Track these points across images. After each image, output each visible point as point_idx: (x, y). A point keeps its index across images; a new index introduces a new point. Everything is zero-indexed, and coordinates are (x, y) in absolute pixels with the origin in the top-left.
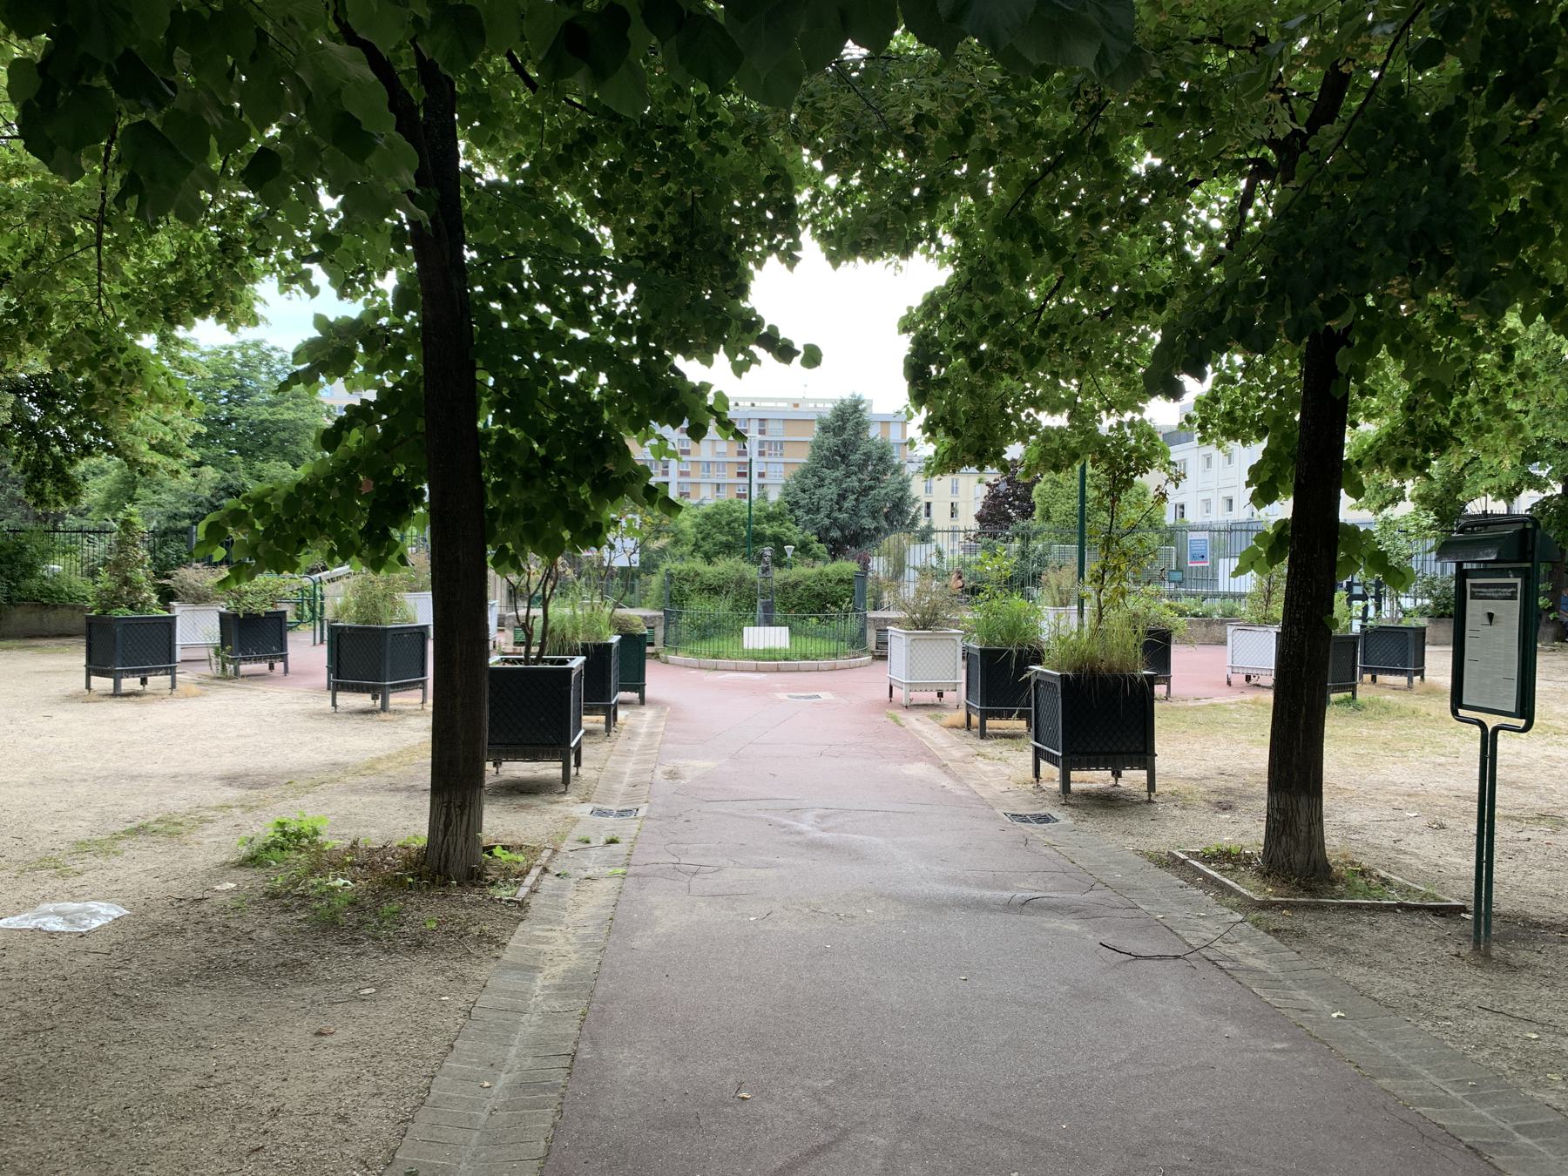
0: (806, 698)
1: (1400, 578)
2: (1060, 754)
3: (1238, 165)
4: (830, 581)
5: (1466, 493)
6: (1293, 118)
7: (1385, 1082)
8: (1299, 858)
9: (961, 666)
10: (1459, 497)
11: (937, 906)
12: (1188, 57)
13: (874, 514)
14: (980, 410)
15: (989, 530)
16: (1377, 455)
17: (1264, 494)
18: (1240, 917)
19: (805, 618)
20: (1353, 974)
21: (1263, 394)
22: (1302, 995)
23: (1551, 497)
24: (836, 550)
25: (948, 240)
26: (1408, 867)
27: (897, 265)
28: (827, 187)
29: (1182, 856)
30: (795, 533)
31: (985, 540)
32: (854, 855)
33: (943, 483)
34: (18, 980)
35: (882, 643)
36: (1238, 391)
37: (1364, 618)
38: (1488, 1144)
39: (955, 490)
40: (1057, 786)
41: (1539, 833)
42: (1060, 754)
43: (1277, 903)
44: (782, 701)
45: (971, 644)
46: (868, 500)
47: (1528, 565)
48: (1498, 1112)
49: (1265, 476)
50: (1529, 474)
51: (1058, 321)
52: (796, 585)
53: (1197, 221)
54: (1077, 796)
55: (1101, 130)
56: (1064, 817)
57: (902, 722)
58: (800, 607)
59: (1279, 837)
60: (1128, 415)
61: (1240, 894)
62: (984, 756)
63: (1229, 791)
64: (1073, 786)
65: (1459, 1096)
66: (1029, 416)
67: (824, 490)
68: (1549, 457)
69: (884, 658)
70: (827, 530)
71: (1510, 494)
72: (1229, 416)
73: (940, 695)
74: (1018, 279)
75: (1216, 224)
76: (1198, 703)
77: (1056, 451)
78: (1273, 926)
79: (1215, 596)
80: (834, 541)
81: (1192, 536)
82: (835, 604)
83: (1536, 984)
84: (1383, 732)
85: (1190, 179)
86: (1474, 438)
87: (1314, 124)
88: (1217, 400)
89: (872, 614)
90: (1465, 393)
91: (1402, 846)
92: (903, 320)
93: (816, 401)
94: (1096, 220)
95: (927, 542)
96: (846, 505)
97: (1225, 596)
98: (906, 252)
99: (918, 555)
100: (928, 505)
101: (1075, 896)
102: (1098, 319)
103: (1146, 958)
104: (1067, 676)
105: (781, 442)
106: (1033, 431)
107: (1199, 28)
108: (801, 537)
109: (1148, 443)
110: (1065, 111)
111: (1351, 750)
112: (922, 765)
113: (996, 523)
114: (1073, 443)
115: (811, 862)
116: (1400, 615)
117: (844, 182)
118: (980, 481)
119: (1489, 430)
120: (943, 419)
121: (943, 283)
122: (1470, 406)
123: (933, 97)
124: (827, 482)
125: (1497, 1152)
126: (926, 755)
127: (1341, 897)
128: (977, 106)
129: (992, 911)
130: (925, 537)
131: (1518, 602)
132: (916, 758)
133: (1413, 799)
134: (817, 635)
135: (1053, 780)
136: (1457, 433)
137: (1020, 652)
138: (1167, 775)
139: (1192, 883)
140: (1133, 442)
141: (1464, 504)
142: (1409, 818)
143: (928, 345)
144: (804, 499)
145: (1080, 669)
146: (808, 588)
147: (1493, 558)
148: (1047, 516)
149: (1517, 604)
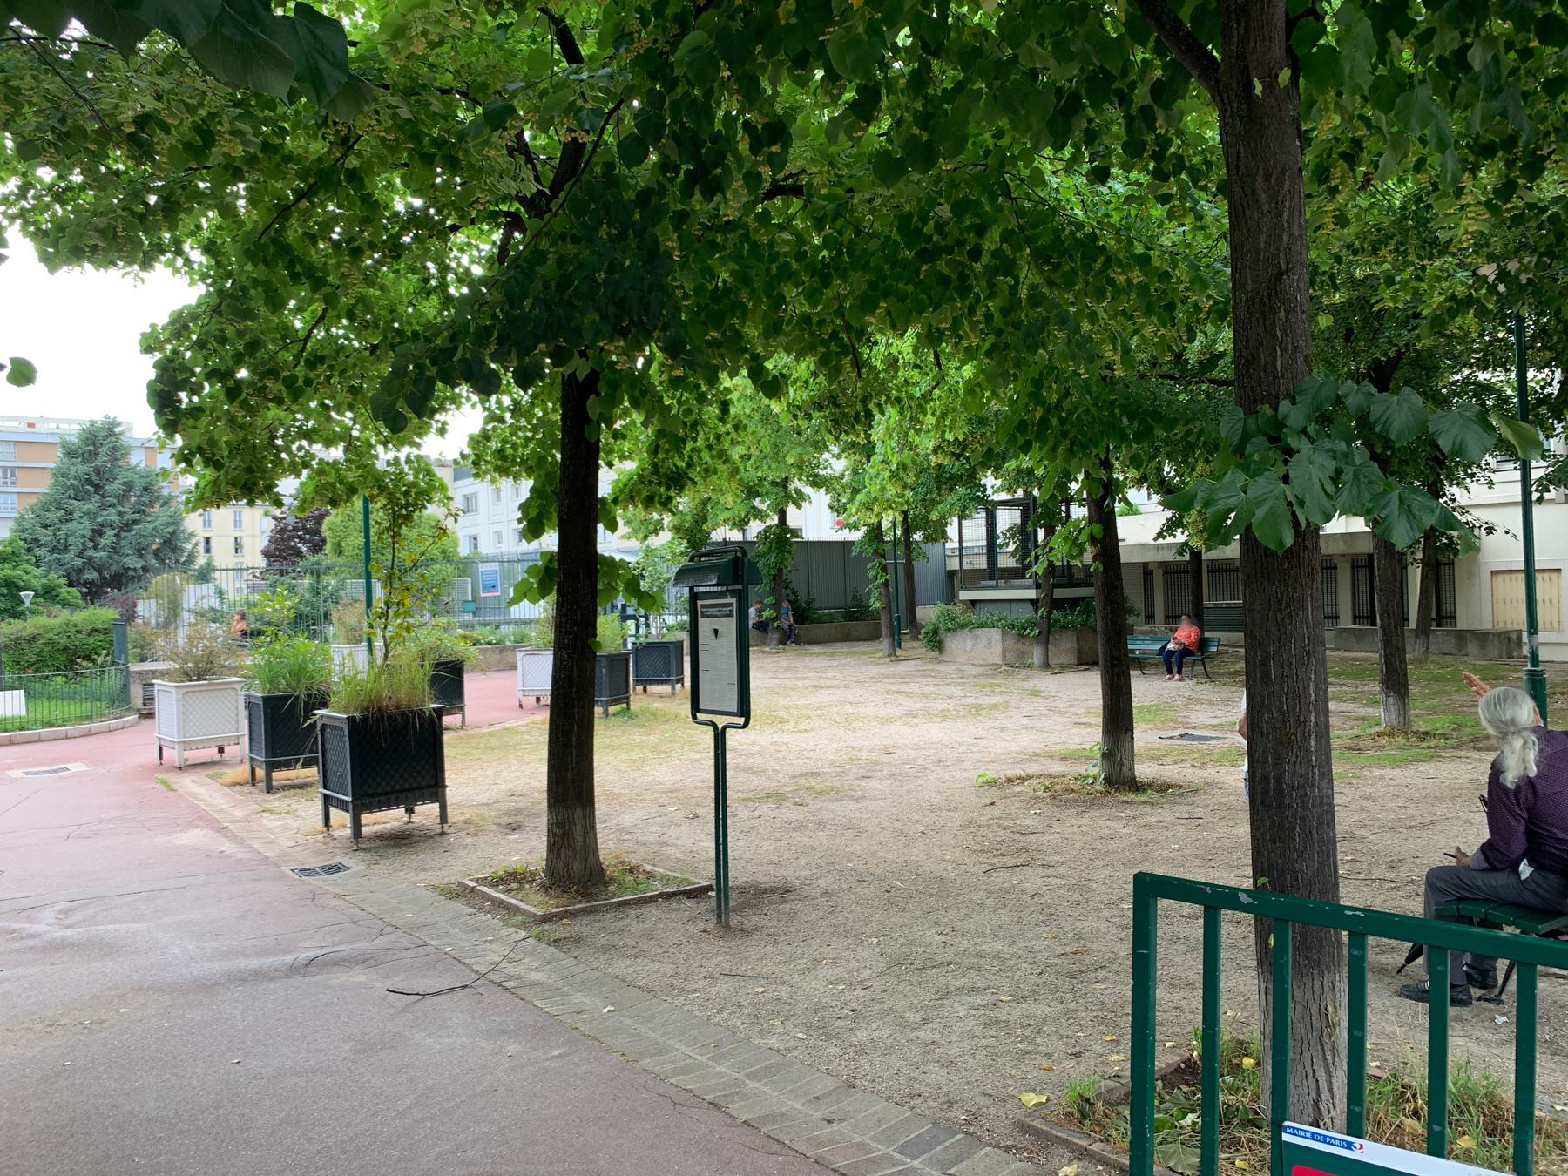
0: (37, 773)
1: (650, 601)
2: (349, 799)
3: (493, 217)
4: (79, 632)
5: (709, 524)
6: (537, 179)
7: (645, 1063)
8: (577, 867)
9: (243, 714)
10: (705, 527)
11: (208, 987)
12: (436, 106)
13: (140, 552)
14: (245, 440)
15: (277, 565)
16: (629, 493)
17: (533, 529)
18: (523, 934)
19: (47, 678)
20: (622, 967)
21: (530, 434)
22: (578, 998)
23: (770, 527)
24: (93, 593)
25: (197, 256)
26: (669, 857)
27: (136, 275)
28: (40, 180)
29: (472, 884)
30: (37, 577)
31: (271, 578)
32: (108, 949)
33: (223, 517)
34: (1060, 699)
35: (149, 699)
36: (508, 431)
37: (637, 635)
38: (725, 1096)
39: (238, 523)
40: (348, 832)
41: (767, 810)
42: (349, 799)
43: (557, 913)
44: (16, 779)
45: (252, 693)
46: (132, 535)
47: (740, 587)
48: (733, 1065)
49: (533, 513)
50: (754, 507)
51: (326, 352)
52: (32, 639)
53: (459, 264)
54: (369, 839)
55: (353, 162)
56: (355, 864)
57: (175, 786)
58: (40, 664)
59: (559, 850)
60: (406, 450)
61: (524, 912)
62: (271, 812)
63: (518, 811)
64: (365, 830)
65: (704, 1059)
66: (300, 448)
67: (73, 525)
68: (767, 493)
69: (151, 715)
70: (80, 571)
71: (741, 524)
72: (500, 453)
73: (221, 750)
74: (277, 304)
75: (477, 271)
76: (492, 729)
77: (333, 485)
78: (554, 937)
79: (508, 623)
80: (89, 584)
81: (482, 567)
82: (87, 658)
83: (763, 943)
84: (652, 737)
85: (449, 223)
86: (704, 479)
87: (556, 186)
88: (488, 439)
89: (135, 667)
90: (695, 440)
91: (665, 839)
92: (144, 336)
93: (58, 421)
94: (357, 253)
95: (207, 581)
96: (102, 542)
97: (517, 623)
98: (146, 264)
99: (195, 596)
100: (208, 540)
101: (365, 945)
102: (367, 353)
103: (438, 993)
104: (354, 718)
105: (13, 469)
106: (306, 465)
107: (447, 79)
108: (44, 581)
109: (427, 478)
110: (316, 138)
111: (626, 757)
112: (197, 831)
113: (285, 559)
114: (351, 476)
115: (48, 968)
116: (665, 631)
117: (61, 177)
118: (266, 514)
119: (715, 472)
120: (200, 450)
121: (194, 302)
122: (699, 451)
123: (159, 98)
124: (76, 515)
125: (732, 1102)
126: (205, 820)
127: (612, 897)
128: (212, 115)
129: (271, 979)
130: (204, 575)
131: (734, 619)
132: (190, 825)
133: (675, 794)
134: (72, 697)
135: (345, 826)
136: (692, 474)
137: (309, 696)
138: (460, 805)
139: (481, 909)
140: (411, 478)
141: (709, 533)
142: (671, 812)
143: (175, 370)
144: (46, 536)
145: (367, 709)
146: (50, 642)
147: (714, 582)
148: (339, 551)
149: (734, 619)
